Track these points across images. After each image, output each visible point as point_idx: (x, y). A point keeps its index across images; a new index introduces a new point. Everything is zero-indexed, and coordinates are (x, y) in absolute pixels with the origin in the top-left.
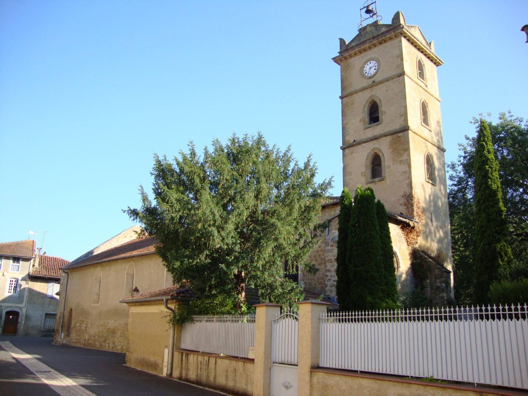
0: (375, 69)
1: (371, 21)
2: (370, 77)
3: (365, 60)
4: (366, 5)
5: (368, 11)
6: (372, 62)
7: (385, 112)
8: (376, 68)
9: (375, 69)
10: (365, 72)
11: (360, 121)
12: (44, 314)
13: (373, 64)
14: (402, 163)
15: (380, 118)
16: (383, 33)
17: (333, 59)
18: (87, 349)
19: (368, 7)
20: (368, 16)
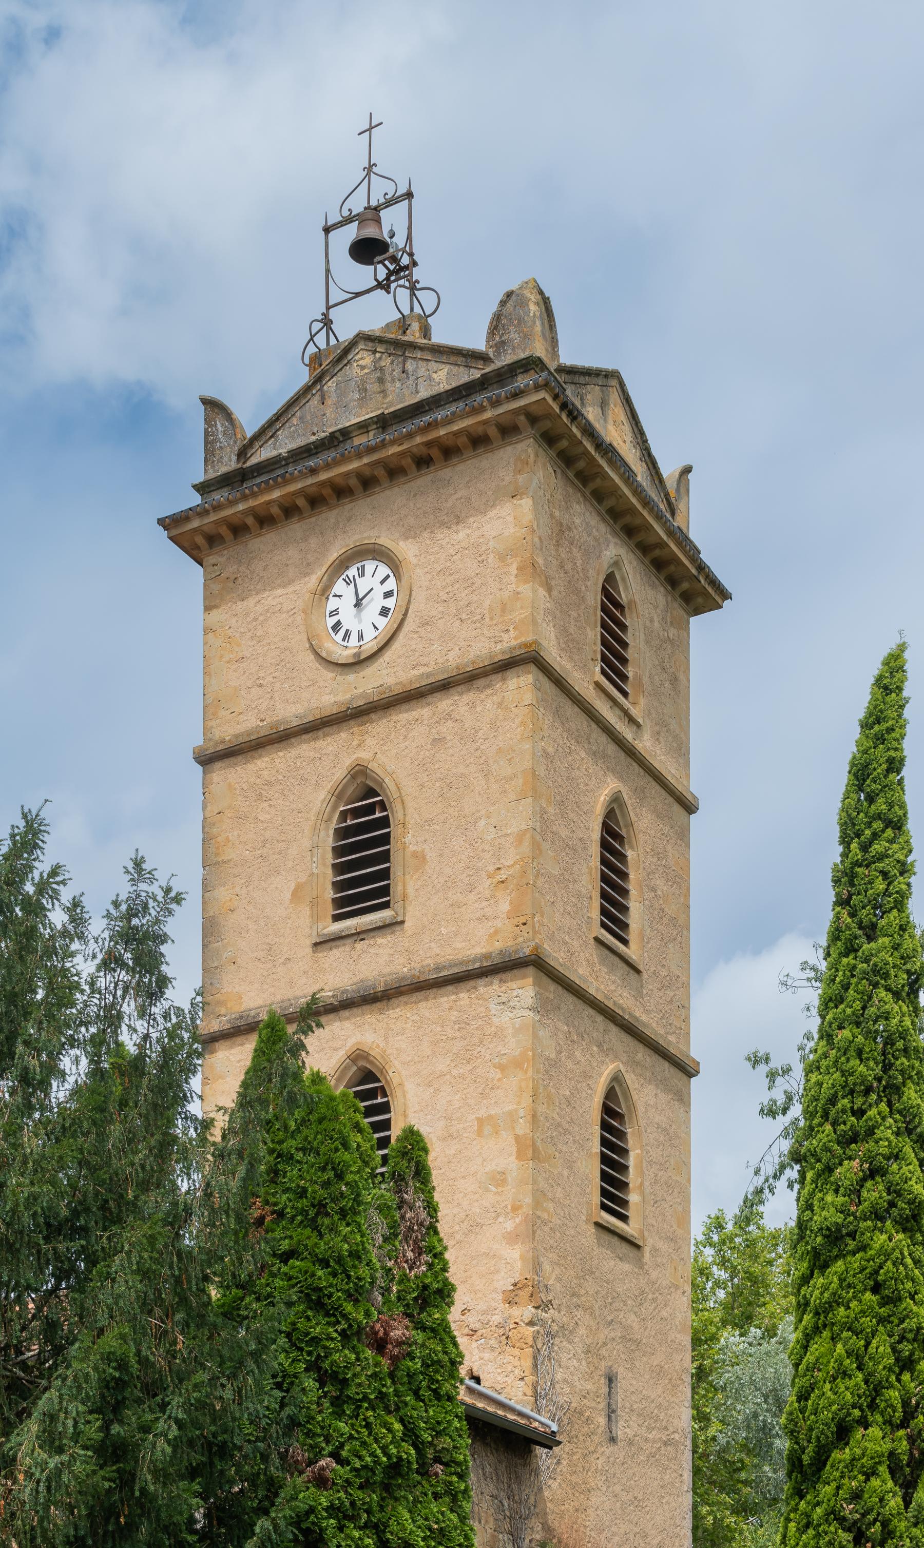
0: (384, 612)
1: (377, 313)
2: (359, 662)
3: (334, 555)
4: (357, 205)
5: (367, 250)
6: (370, 566)
7: (420, 857)
8: (390, 603)
9: (384, 612)
10: (331, 622)
11: (296, 895)
12: (331, 631)
13: (373, 576)
14: (487, 1130)
15: (397, 889)
16: (436, 401)
17: (194, 487)
18: (825, 1465)
19: (373, 214)
20: (365, 275)
